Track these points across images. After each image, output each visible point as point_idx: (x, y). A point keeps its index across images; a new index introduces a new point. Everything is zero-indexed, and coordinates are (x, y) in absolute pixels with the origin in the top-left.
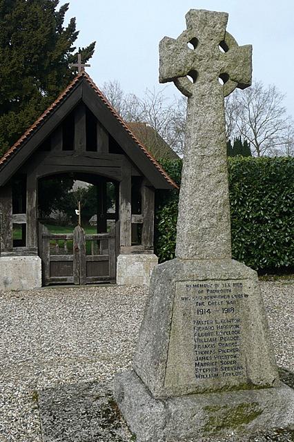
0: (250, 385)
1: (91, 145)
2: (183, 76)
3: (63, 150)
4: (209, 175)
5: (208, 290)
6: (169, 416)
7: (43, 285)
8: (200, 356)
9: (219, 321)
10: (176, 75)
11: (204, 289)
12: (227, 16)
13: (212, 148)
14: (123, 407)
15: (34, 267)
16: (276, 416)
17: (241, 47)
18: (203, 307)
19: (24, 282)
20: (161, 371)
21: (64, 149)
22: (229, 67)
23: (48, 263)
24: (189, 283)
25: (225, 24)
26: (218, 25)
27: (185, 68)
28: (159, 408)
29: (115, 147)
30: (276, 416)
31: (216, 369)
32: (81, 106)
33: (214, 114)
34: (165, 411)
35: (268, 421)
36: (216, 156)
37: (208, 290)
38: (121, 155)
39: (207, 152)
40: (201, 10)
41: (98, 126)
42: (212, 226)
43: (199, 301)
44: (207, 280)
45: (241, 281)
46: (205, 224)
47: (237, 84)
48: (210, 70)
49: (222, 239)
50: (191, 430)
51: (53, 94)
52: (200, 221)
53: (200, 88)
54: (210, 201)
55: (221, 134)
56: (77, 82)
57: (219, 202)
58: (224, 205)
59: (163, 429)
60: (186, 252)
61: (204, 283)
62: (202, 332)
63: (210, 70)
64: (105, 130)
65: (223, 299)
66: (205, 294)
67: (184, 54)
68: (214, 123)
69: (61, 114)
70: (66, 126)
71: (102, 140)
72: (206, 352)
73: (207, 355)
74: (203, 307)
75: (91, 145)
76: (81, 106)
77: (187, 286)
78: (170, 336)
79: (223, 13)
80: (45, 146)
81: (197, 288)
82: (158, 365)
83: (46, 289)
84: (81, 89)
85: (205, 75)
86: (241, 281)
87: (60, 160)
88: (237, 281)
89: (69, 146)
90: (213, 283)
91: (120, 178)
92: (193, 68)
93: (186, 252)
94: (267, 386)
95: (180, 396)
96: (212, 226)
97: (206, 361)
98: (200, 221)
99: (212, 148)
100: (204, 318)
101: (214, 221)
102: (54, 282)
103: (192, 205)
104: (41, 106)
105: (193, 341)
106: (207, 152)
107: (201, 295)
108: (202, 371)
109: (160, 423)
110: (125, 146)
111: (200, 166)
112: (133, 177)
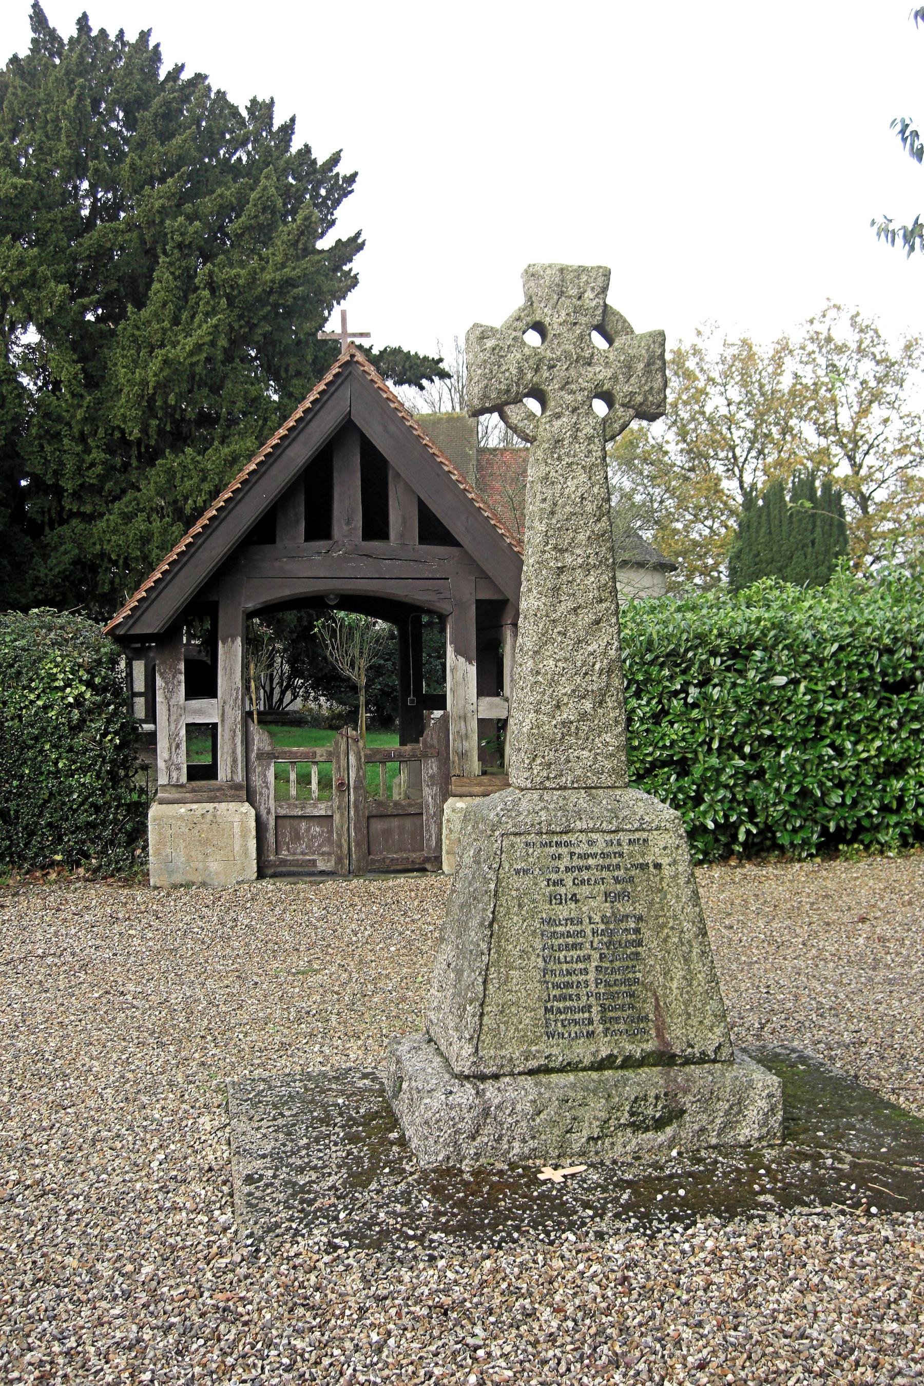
0: (665, 1058)
1: (375, 526)
2: (517, 400)
3: (306, 540)
4: (575, 609)
5: (572, 854)
6: (486, 1113)
7: (261, 875)
8: (556, 992)
9: (597, 919)
10: (499, 401)
11: (564, 851)
12: (607, 274)
13: (578, 551)
14: (400, 1107)
15: (237, 830)
16: (718, 1121)
17: (642, 337)
18: (563, 891)
19: (214, 866)
20: (471, 1021)
21: (309, 537)
22: (614, 378)
23: (272, 823)
24: (532, 838)
25: (605, 289)
26: (589, 294)
27: (518, 385)
28: (465, 1095)
29: (432, 530)
30: (718, 1121)
31: (591, 1022)
32: (348, 428)
33: (583, 478)
34: (477, 1102)
35: (703, 1130)
36: (587, 569)
37: (572, 854)
38: (454, 549)
39: (568, 559)
40: (550, 266)
41: (132, 632)
42: (583, 716)
43: (554, 876)
44: (570, 831)
45: (645, 835)
46: (567, 714)
47: (631, 412)
48: (573, 387)
49: (607, 744)
50: (532, 1144)
51: (291, 397)
52: (558, 707)
53: (553, 426)
54: (579, 664)
55: (599, 520)
56: (337, 376)
57: (597, 667)
58: (610, 672)
59: (474, 1139)
60: (527, 774)
61: (565, 838)
62: (561, 941)
63: (573, 387)
64: (409, 489)
65: (604, 874)
66: (563, 864)
67: (516, 356)
68: (582, 498)
69: (300, 454)
70: (314, 483)
71: (400, 517)
72: (568, 985)
73: (570, 991)
74: (563, 891)
75: (375, 526)
76: (348, 428)
77: (527, 844)
78: (490, 950)
79: (600, 267)
80: (264, 532)
81: (547, 849)
82: (465, 1009)
83: (268, 885)
84: (346, 392)
85: (562, 397)
86: (645, 835)
87: (301, 567)
88: (637, 835)
89: (319, 527)
90: (583, 837)
91: (445, 607)
92: (537, 384)
93: (527, 774)
94: (703, 1059)
95: (512, 1074)
96: (583, 716)
97: (568, 1004)
98: (558, 707)
99: (578, 551)
100: (563, 912)
101: (588, 705)
102: (284, 869)
103: (538, 673)
104: (264, 417)
105: (540, 960)
106: (568, 559)
107: (556, 863)
108: (559, 1024)
109: (466, 1126)
110: (457, 529)
111: (556, 590)
112: (480, 604)
